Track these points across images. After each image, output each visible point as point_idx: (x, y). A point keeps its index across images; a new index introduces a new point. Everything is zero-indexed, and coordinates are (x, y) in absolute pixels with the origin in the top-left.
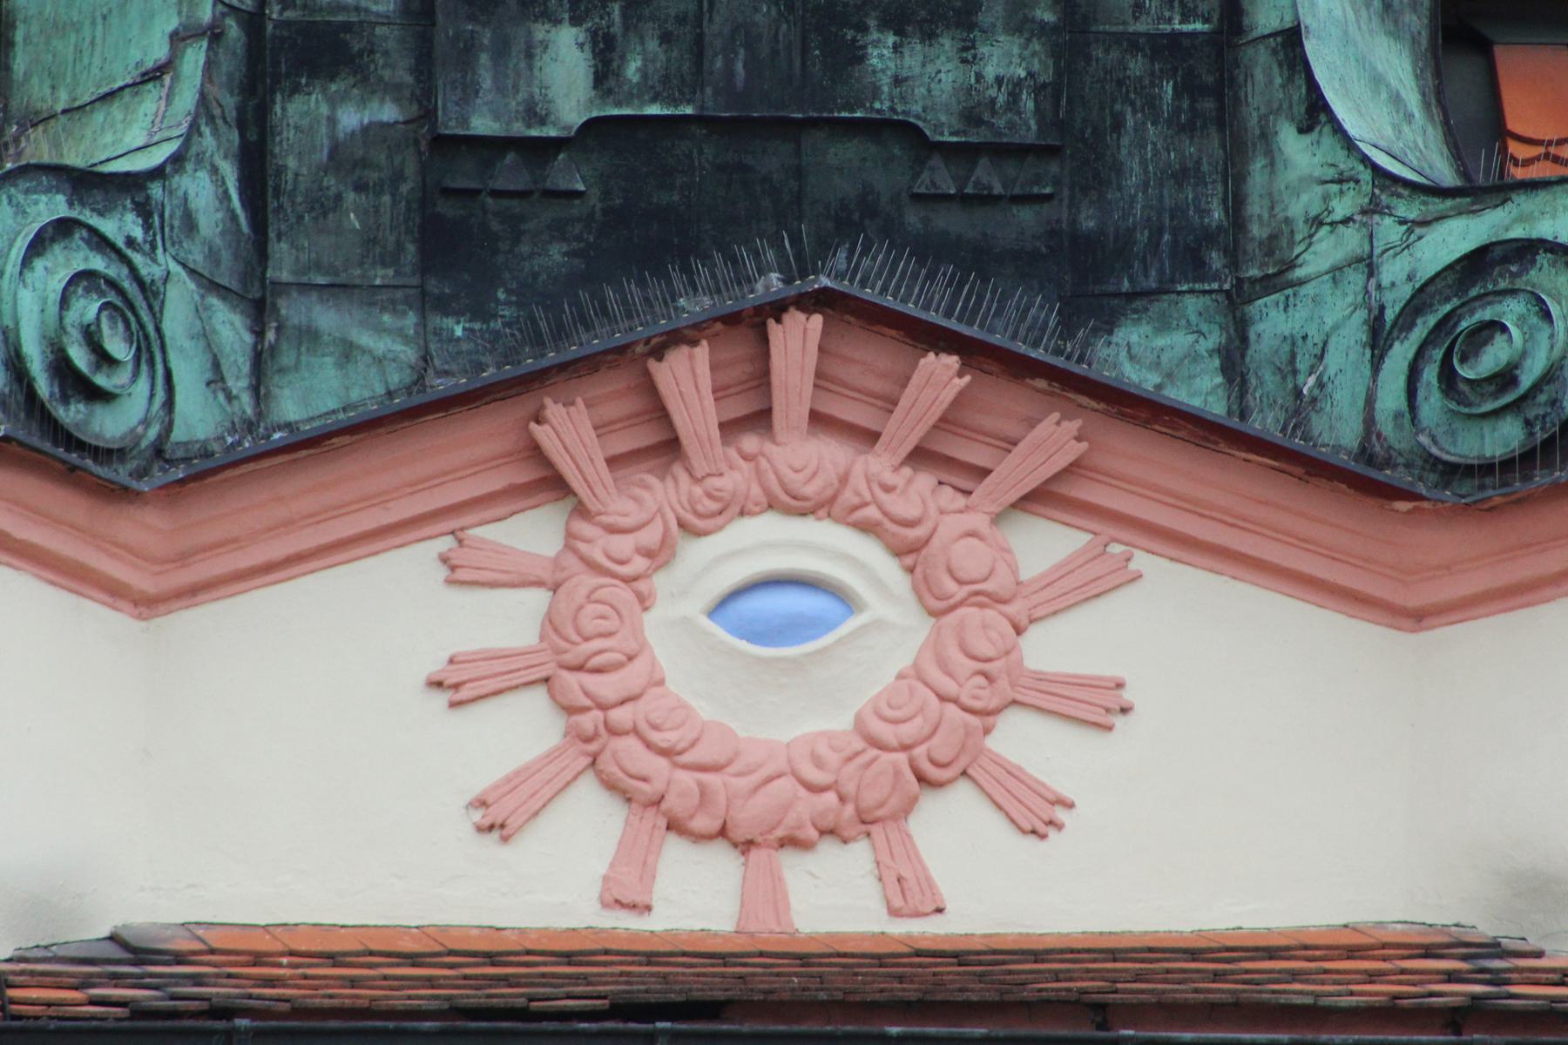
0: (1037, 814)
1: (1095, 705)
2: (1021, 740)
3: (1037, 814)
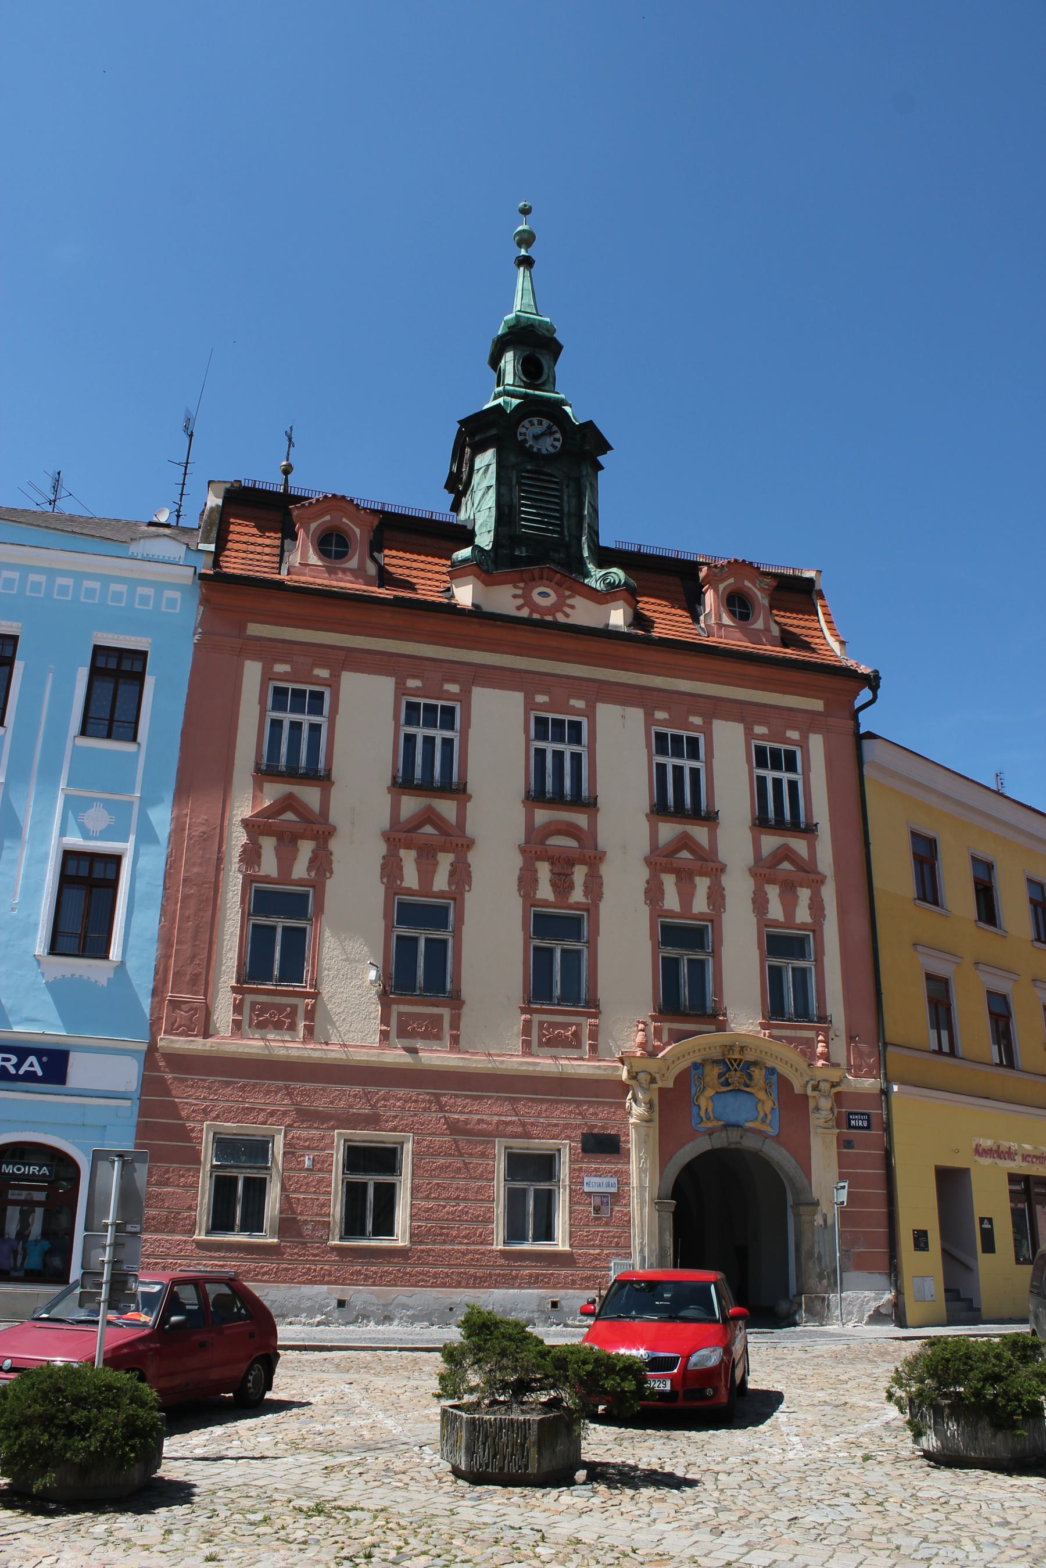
0: (567, 615)
1: (572, 607)
2: (567, 610)
3: (567, 615)
